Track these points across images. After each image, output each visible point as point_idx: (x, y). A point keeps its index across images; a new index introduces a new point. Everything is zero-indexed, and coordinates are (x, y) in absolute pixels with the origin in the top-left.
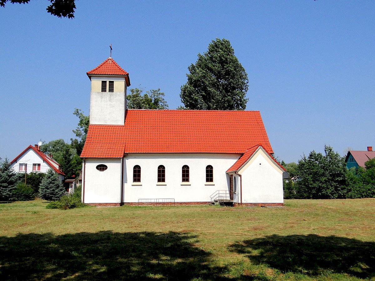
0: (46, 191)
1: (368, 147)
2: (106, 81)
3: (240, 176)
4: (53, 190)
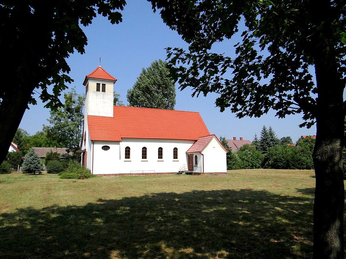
0: (30, 166)
1: (240, 138)
2: (100, 84)
3: (203, 155)
4: (37, 165)
